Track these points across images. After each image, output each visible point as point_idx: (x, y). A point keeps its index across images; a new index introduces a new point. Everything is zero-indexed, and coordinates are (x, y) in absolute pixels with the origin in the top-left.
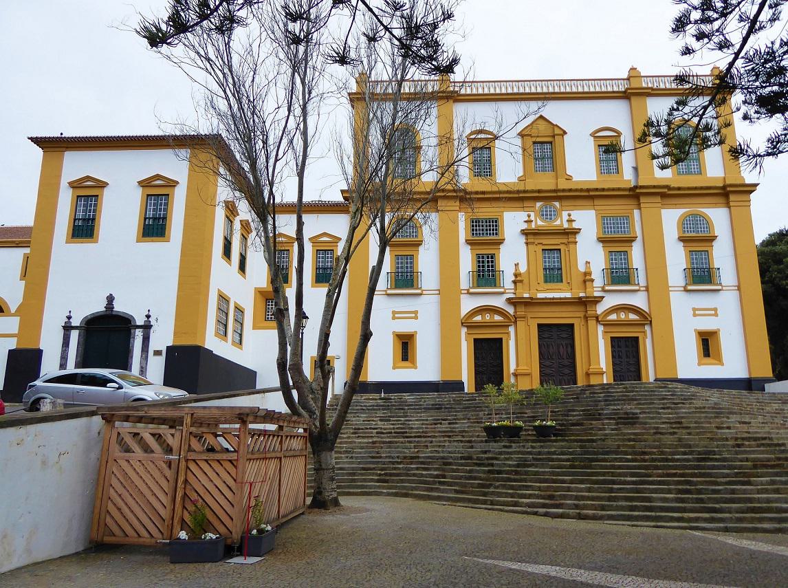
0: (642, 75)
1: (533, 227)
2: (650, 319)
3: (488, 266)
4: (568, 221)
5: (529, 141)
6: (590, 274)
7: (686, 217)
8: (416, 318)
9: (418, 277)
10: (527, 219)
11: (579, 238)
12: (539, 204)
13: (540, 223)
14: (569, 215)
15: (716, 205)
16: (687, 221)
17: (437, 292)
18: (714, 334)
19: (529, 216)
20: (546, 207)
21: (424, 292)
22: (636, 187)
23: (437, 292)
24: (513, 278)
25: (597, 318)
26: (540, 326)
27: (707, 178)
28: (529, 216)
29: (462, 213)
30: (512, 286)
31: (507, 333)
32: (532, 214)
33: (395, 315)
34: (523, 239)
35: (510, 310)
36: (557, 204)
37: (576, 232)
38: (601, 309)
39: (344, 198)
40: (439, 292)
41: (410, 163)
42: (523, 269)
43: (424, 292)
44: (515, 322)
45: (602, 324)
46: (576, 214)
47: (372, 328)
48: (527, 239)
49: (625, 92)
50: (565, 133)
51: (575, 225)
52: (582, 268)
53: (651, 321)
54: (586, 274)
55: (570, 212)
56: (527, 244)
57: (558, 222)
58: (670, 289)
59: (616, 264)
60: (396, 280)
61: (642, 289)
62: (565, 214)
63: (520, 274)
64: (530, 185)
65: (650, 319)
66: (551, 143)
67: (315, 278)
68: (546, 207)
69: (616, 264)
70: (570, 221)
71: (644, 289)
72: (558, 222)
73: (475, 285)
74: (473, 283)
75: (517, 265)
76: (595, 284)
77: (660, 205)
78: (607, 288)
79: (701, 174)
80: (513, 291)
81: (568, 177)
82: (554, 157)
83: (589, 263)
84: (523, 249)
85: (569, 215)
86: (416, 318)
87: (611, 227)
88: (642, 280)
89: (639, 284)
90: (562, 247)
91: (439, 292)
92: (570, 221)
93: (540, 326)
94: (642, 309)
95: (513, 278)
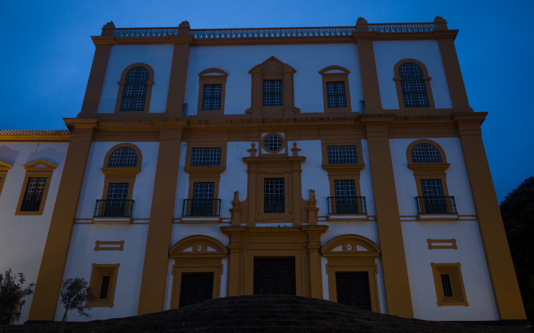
0: (368, 23)
3: (277, 191)
4: (293, 150)
6: (315, 202)
7: (416, 146)
8: (121, 249)
9: (216, 204)
10: (250, 147)
13: (264, 152)
14: (295, 145)
16: (416, 150)
17: (77, 221)
18: (455, 268)
19: (253, 145)
21: (461, 218)
22: (361, 116)
23: (474, 218)
24: (231, 207)
25: (320, 250)
27: (224, 115)
28: (253, 145)
29: (184, 143)
30: (229, 215)
34: (245, 167)
35: (224, 240)
38: (324, 238)
39: (68, 127)
40: (477, 217)
41: (332, 96)
42: (243, 197)
43: (461, 218)
44: (228, 254)
45: (325, 257)
47: (433, 250)
48: (249, 168)
49: (352, 37)
51: (300, 154)
53: (380, 254)
54: (308, 203)
56: (249, 172)
57: (283, 151)
58: (401, 219)
59: (342, 193)
60: (337, 206)
61: (370, 218)
62: (290, 144)
63: (240, 203)
65: (379, 251)
66: (281, 81)
67: (41, 206)
69: (342, 193)
71: (176, 221)
72: (283, 151)
73: (335, 211)
74: (333, 209)
75: (236, 193)
76: (320, 214)
78: (331, 217)
79: (429, 106)
80: (229, 220)
82: (283, 93)
83: (314, 191)
84: (244, 177)
85: (295, 145)
86: (121, 249)
87: (351, 156)
88: (370, 211)
89: (366, 213)
92: (295, 150)
94: (366, 238)
95: (231, 207)
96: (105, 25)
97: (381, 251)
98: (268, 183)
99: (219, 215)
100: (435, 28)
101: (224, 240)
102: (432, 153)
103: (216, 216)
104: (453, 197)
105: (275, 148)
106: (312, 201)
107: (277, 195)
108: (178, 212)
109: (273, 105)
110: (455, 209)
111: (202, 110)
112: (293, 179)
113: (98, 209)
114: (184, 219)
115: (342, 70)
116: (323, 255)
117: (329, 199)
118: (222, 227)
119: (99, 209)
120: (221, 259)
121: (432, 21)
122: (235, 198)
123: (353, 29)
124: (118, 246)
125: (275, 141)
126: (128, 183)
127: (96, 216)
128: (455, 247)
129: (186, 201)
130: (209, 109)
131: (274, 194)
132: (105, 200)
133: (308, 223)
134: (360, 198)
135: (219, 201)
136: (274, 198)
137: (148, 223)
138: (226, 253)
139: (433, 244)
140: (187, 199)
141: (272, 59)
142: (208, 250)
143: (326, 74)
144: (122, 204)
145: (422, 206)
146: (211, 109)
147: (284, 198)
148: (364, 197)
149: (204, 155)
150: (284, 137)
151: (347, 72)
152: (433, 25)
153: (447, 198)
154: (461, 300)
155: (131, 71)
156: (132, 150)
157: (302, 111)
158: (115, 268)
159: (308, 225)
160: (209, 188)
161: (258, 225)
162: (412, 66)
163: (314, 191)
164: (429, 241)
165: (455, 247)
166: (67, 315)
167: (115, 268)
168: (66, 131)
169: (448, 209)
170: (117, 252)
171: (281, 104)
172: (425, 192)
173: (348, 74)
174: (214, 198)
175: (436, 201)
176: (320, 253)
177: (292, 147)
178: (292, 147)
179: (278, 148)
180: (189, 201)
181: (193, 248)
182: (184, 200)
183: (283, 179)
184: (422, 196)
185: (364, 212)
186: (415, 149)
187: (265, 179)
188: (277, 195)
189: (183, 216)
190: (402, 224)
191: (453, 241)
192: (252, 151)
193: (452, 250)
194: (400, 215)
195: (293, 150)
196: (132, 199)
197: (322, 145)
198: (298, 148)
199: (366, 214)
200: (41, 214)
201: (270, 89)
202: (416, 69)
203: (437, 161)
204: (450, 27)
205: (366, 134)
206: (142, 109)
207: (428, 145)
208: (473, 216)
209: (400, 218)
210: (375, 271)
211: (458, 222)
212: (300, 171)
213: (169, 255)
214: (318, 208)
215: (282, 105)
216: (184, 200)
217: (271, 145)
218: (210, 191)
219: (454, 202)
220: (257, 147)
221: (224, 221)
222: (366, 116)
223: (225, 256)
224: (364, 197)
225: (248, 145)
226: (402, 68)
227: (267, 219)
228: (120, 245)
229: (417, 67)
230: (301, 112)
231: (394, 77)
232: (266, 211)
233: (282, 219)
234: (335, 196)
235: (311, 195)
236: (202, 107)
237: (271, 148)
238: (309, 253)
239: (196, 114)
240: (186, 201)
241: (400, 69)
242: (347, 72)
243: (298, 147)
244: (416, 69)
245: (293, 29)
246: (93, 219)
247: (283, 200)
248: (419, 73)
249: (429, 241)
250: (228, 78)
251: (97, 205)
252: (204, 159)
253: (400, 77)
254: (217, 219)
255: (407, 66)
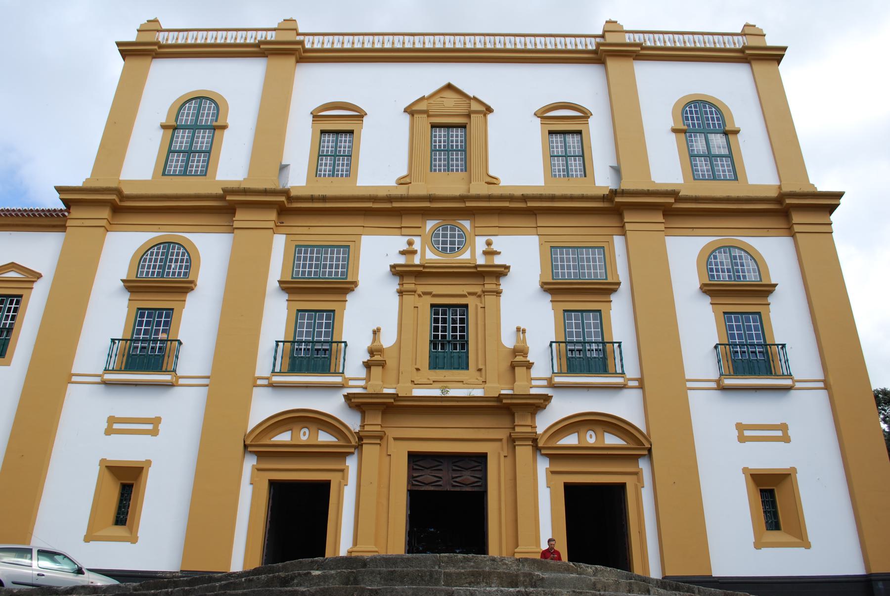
0: (625, 28)
1: (417, 260)
2: (647, 445)
4: (485, 253)
5: (424, 123)
8: (154, 432)
9: (338, 351)
10: (405, 247)
11: (505, 284)
12: (430, 224)
14: (489, 243)
15: (767, 232)
19: (410, 243)
20: (445, 229)
22: (614, 193)
24: (367, 357)
26: (414, 458)
28: (410, 243)
30: (363, 373)
31: (342, 471)
32: (417, 241)
33: (113, 426)
34: (394, 285)
35: (353, 422)
36: (466, 224)
37: (501, 272)
42: (388, 340)
46: (500, 242)
48: (401, 284)
50: (489, 110)
51: (498, 260)
52: (508, 340)
53: (650, 450)
54: (516, 352)
55: (493, 238)
56: (401, 293)
57: (466, 256)
64: (418, 189)
65: (647, 445)
66: (463, 126)
68: (445, 229)
70: (489, 253)
73: (565, 368)
75: (376, 332)
77: (662, 227)
81: (489, 180)
83: (524, 331)
85: (489, 243)
86: (154, 432)
88: (631, 370)
89: (623, 373)
90: (471, 301)
91: (69, 378)
92: (489, 253)
93: (414, 458)
95: (367, 357)
96: (143, 23)
97: (651, 445)
98: (437, 313)
99: (343, 373)
100: (744, 43)
101: (353, 422)
102: (715, 271)
103: (336, 373)
104: (783, 346)
105: (452, 250)
106: (520, 351)
107: (455, 337)
108: (263, 366)
109: (448, 171)
110: (788, 368)
111: (316, 176)
112: (484, 307)
113: (113, 355)
114: (276, 379)
115: (579, 112)
116: (540, 451)
117: (554, 345)
118: (348, 394)
119: (116, 355)
120: (344, 455)
121: (739, 31)
122: (374, 340)
123: (598, 40)
124: (150, 427)
125: (445, 243)
126: (172, 309)
127: (109, 369)
128: (786, 439)
129: (279, 343)
130: (329, 175)
131: (449, 334)
132: (127, 340)
133: (513, 389)
134: (611, 344)
135: (343, 345)
136: (449, 342)
137: (207, 385)
138: (353, 443)
139: (747, 433)
140: (283, 340)
141: (449, 87)
142: (319, 439)
143: (545, 116)
144: (160, 348)
145: (728, 361)
146: (333, 176)
147: (467, 342)
148: (620, 343)
149: (318, 259)
150: (469, 229)
151: (585, 115)
152: (740, 37)
153: (772, 347)
154: (800, 538)
155: (187, 105)
156: (182, 248)
157: (503, 183)
158: (142, 468)
159: (513, 393)
160: (324, 321)
161: (417, 392)
162: (705, 107)
163: (524, 331)
164: (740, 427)
165: (786, 439)
166: (14, 583)
167: (142, 468)
168: (61, 210)
169: (729, 367)
170: (148, 437)
171: (466, 168)
172: (733, 336)
173: (589, 117)
174: (334, 340)
175: (752, 352)
176: (536, 448)
177: (485, 248)
178: (485, 248)
179: (458, 248)
180: (285, 343)
181: (254, 374)
182: (277, 342)
183: (466, 306)
184: (727, 343)
185: (619, 370)
186: (712, 256)
187: (432, 306)
188: (455, 337)
189: (273, 371)
190: (690, 393)
191: (784, 427)
192: (409, 253)
193: (781, 444)
194: (687, 377)
195: (485, 253)
196: (178, 339)
197: (541, 245)
198: (495, 250)
199: (623, 375)
200: (8, 365)
201: (444, 142)
202: (711, 113)
203: (742, 278)
204: (770, 41)
205: (623, 227)
206: (204, 174)
207: (440, 250)
208: (208, 377)
209: (532, 381)
210: (640, 484)
211: (176, 389)
212: (498, 293)
213: (246, 446)
214: (531, 361)
215: (466, 171)
216: (277, 342)
217: (445, 243)
218: (328, 326)
219: (785, 354)
220: (417, 246)
221: (351, 383)
222: (624, 193)
223: (352, 450)
224: (620, 343)
225: (399, 242)
226: (687, 110)
227: (433, 381)
228: (153, 426)
229: (713, 109)
230: (500, 185)
231: (673, 125)
232: (434, 364)
233: (463, 382)
234: (563, 340)
235: (518, 337)
236: (316, 172)
237: (444, 250)
238: (514, 447)
239: (304, 184)
240: (281, 344)
241: (684, 111)
242: (585, 115)
243: (494, 247)
244: (711, 113)
245: (488, 37)
246: (103, 376)
247: (464, 344)
248: (718, 119)
249: (740, 427)
250: (365, 119)
251: (111, 349)
252: (317, 266)
253: (684, 125)
254: (338, 379)
255: (695, 107)
